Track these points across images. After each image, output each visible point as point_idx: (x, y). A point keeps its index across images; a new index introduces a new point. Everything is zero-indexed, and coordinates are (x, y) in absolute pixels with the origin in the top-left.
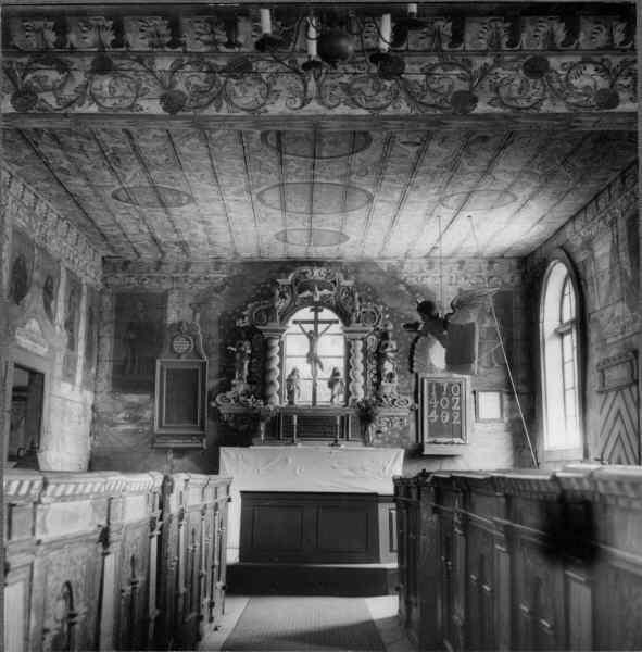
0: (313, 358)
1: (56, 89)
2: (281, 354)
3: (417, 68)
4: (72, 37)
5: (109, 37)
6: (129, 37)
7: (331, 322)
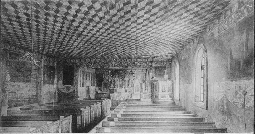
1: (91, 66)
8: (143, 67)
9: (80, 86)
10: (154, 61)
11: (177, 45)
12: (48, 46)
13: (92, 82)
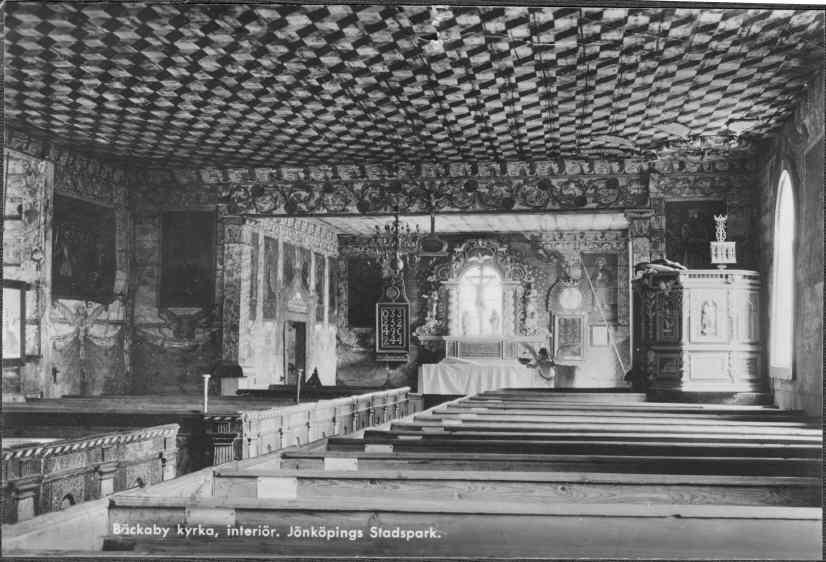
0: (480, 303)
1: (306, 201)
2: (458, 300)
3: (484, 186)
4: (312, 175)
5: (330, 175)
6: (341, 174)
7: (491, 277)
8: (594, 205)
9: (253, 316)
10: (655, 171)
11: (775, 59)
12: (67, 77)
13: (321, 302)
